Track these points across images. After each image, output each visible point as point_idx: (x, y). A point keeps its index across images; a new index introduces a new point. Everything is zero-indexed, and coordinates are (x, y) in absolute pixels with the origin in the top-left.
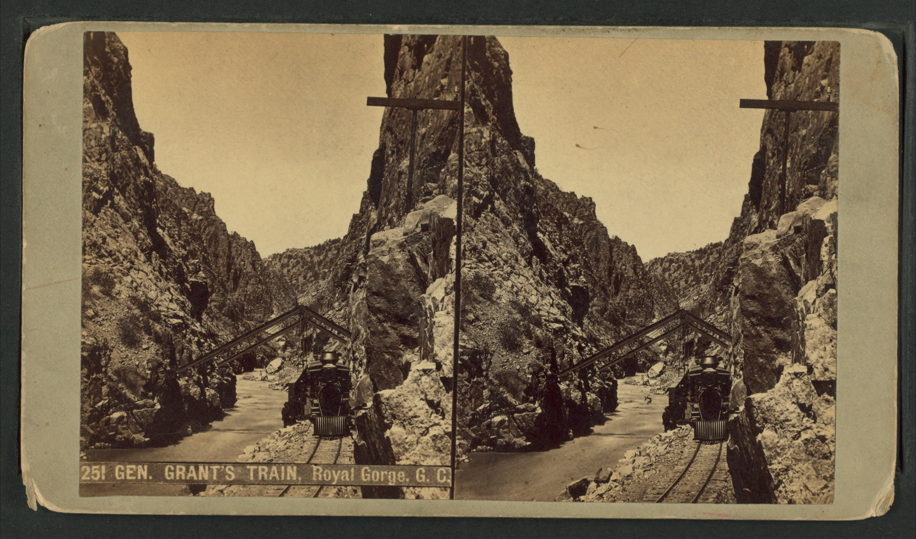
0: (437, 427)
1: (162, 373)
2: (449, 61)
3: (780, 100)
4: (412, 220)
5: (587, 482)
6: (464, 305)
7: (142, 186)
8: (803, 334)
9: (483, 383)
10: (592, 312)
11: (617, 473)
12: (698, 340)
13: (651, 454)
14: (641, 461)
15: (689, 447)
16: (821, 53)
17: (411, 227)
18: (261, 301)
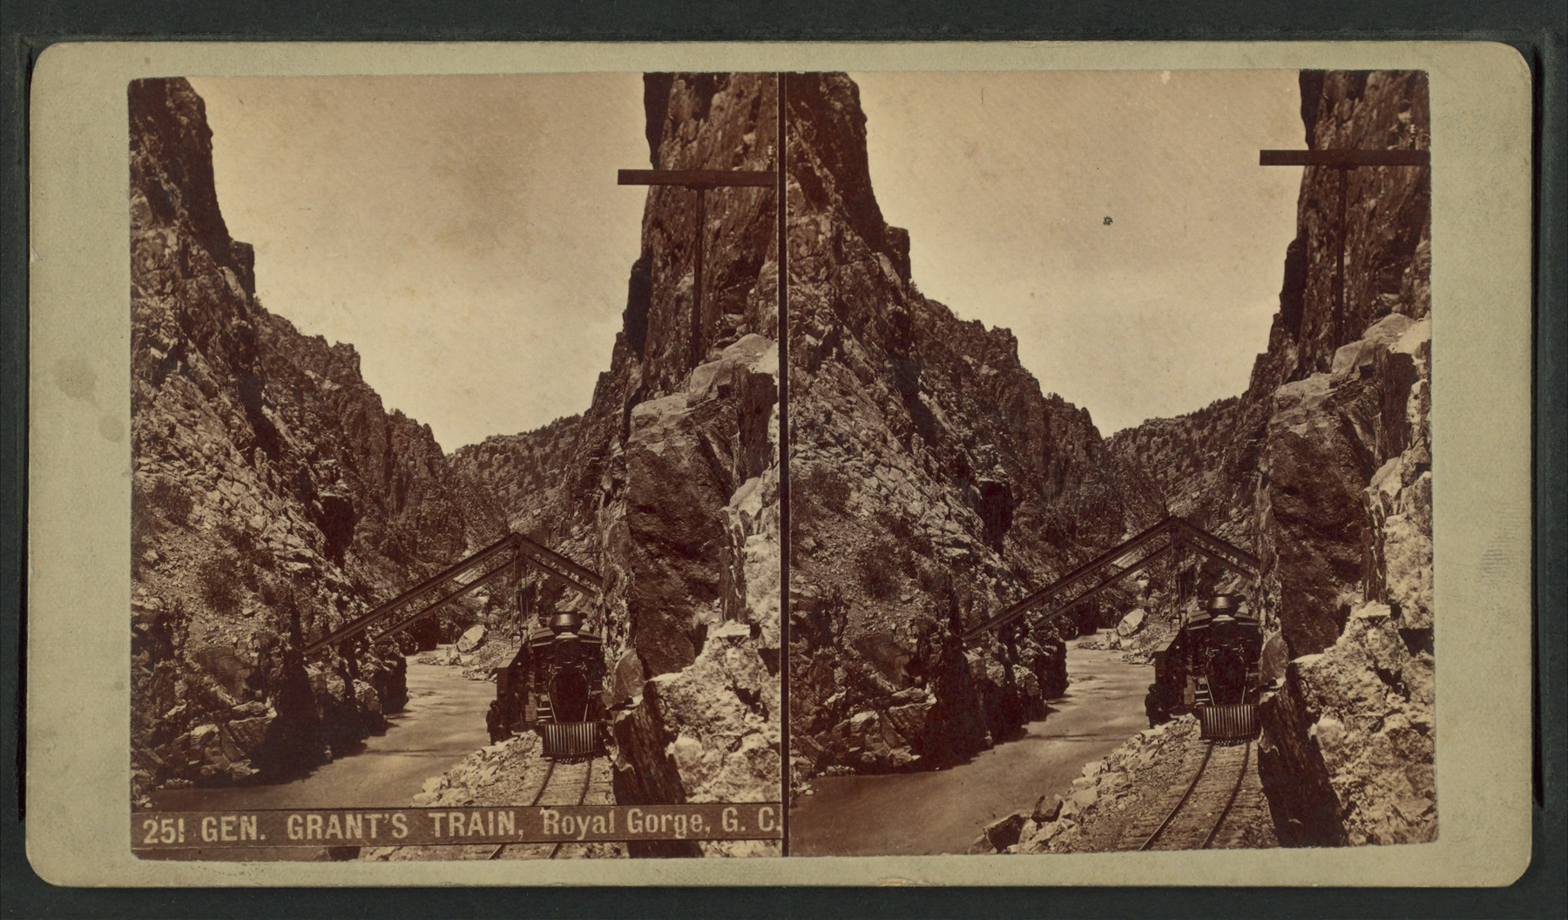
0: (1398, 716)
1: (279, 655)
2: (756, 103)
3: (1329, 150)
4: (701, 380)
5: (1020, 821)
6: (796, 523)
7: (235, 335)
8: (1382, 550)
9: (831, 657)
10: (1017, 527)
11: (1071, 803)
12: (543, 584)
13: (1128, 767)
14: (1110, 780)
15: (1193, 752)
16: (743, 88)
17: (701, 391)
18: (446, 527)
